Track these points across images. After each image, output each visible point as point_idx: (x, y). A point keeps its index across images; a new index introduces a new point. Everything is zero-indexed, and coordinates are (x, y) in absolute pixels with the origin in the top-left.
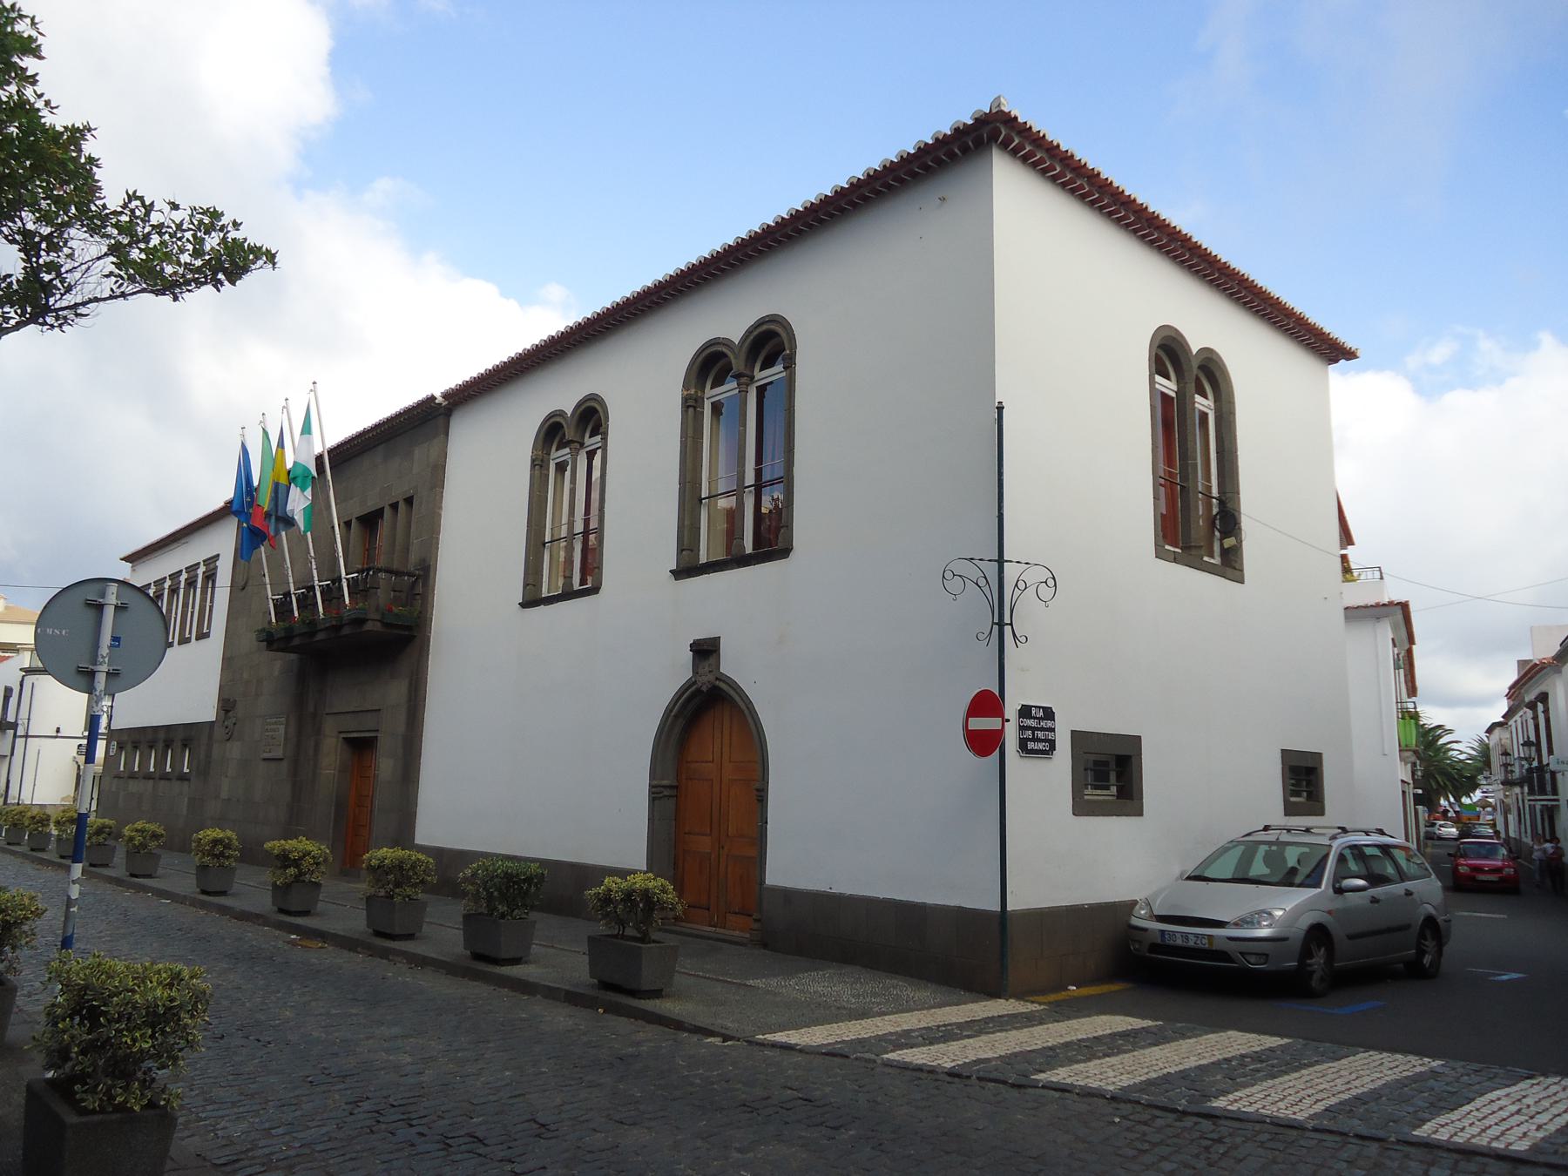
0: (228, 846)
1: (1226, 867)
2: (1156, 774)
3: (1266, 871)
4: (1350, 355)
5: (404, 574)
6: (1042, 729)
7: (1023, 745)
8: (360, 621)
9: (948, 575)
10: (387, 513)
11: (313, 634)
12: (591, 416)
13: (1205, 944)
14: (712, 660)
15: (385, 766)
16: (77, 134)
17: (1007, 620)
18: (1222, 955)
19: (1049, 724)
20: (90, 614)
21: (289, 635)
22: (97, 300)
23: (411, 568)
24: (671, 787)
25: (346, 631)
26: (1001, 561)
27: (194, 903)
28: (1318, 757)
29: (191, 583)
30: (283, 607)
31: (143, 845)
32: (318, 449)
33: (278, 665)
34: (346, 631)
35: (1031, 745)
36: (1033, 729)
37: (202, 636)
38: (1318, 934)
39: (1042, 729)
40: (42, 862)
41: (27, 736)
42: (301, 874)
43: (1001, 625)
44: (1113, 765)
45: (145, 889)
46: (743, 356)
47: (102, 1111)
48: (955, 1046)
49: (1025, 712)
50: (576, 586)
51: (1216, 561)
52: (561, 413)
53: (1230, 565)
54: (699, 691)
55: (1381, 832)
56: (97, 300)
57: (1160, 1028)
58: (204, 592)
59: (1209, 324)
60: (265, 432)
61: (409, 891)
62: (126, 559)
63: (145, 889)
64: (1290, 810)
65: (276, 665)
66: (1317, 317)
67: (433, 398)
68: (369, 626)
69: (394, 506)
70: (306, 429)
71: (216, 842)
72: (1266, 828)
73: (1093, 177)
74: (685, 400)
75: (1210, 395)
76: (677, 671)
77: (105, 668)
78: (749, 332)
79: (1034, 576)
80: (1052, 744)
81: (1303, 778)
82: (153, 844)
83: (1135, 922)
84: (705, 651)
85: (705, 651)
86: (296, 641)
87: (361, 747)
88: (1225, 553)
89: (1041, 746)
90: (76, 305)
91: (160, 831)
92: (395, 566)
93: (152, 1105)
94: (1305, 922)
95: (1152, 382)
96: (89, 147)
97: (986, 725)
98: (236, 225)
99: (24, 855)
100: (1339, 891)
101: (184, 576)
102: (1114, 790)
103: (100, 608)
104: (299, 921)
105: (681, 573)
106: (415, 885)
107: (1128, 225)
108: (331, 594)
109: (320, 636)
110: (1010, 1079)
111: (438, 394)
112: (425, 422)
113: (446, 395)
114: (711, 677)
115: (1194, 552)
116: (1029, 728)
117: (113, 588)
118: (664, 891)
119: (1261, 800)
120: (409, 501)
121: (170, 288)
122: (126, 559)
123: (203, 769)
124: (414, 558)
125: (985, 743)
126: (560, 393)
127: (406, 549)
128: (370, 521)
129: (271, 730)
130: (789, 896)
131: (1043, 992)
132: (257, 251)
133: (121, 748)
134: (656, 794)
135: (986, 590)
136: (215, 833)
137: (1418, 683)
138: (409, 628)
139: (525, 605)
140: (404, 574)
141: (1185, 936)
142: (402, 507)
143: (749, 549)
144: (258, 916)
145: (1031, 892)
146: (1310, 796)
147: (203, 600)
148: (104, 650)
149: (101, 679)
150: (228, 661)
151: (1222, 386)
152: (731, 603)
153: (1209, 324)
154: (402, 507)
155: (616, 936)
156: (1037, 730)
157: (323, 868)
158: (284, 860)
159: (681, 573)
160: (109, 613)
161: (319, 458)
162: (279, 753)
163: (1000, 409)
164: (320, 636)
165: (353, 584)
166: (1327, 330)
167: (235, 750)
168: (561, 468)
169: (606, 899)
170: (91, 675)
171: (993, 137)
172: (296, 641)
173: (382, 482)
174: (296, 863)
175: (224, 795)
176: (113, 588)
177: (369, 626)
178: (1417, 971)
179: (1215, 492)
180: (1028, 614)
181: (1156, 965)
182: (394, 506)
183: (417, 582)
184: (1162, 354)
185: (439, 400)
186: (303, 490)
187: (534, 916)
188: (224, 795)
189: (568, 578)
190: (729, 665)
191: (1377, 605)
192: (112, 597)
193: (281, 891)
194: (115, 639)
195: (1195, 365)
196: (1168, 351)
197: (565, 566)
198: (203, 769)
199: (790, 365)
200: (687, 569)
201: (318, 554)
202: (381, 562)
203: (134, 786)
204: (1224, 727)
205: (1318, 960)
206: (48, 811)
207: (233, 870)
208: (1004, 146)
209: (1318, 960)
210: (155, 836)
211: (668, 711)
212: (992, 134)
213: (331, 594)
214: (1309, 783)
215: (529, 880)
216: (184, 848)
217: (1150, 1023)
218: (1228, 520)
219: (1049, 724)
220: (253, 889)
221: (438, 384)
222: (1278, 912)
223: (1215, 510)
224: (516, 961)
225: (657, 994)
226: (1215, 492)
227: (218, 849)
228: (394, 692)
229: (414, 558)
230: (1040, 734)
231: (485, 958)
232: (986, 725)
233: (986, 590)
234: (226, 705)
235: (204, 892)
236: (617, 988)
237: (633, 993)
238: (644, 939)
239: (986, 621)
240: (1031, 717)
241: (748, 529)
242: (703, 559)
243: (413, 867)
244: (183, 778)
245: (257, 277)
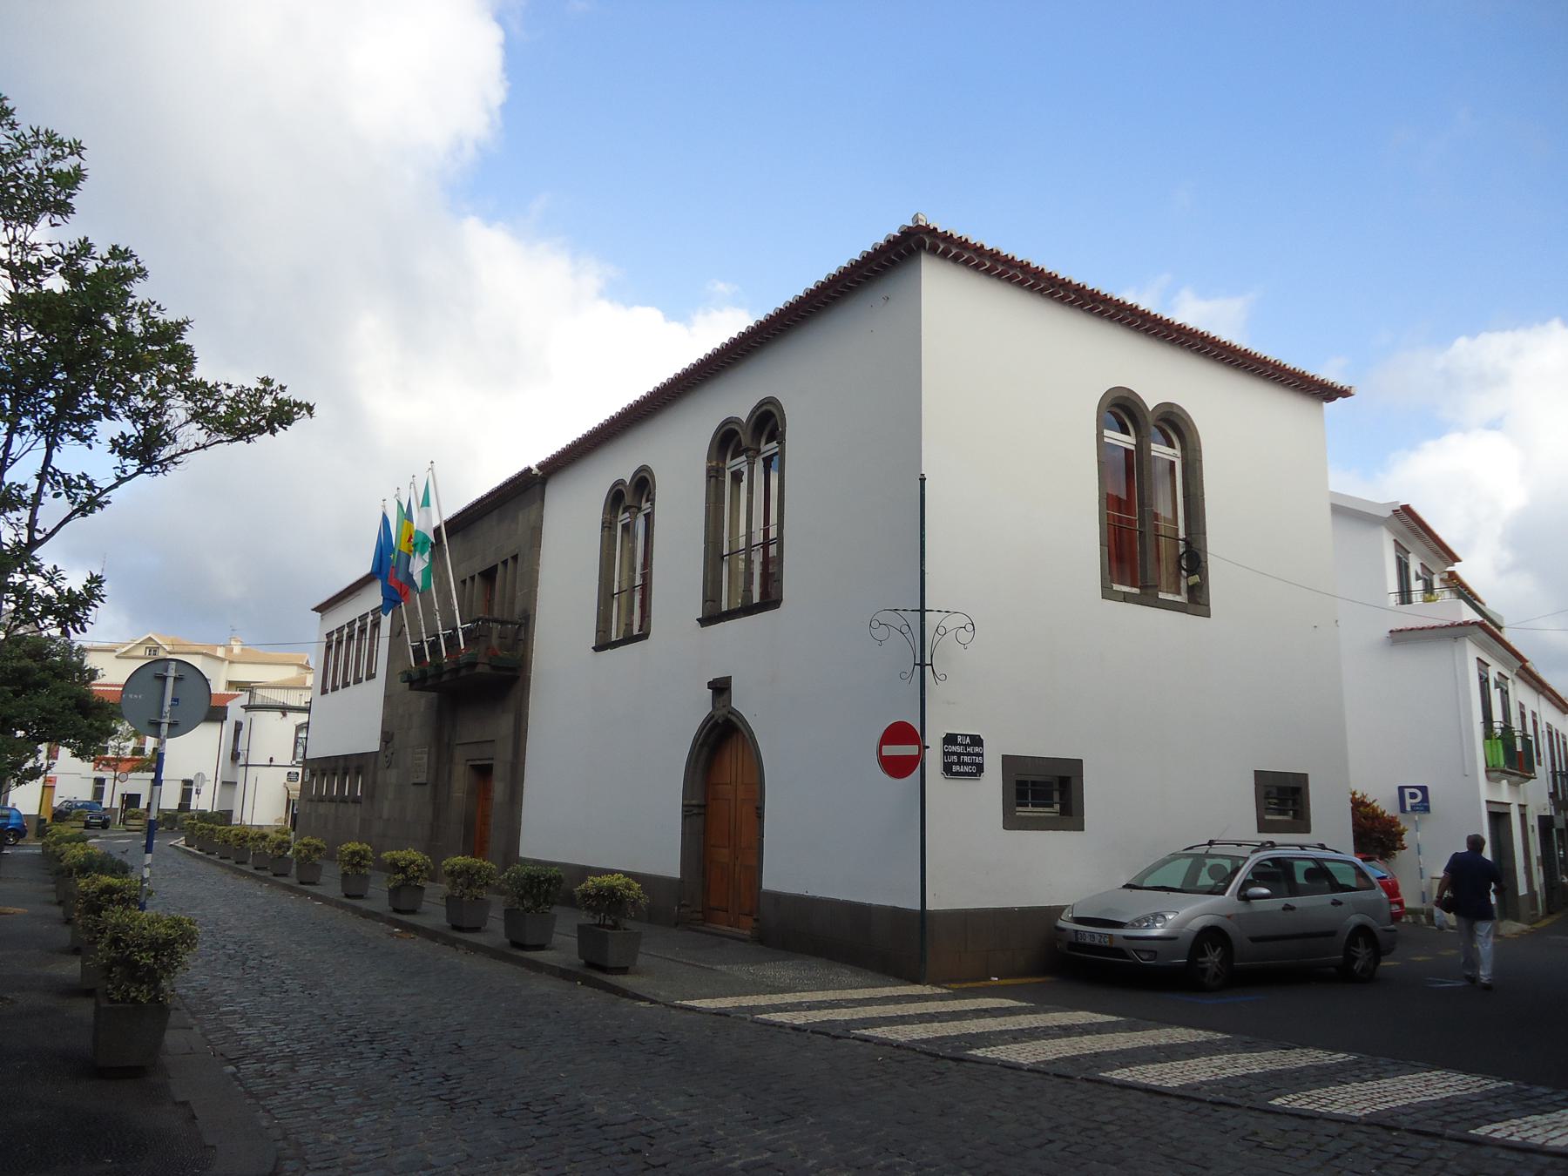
0: (363, 857)
1: (1175, 878)
2: (1094, 792)
3: (1212, 882)
4: (1345, 393)
5: (508, 623)
6: (969, 754)
7: (947, 769)
8: (472, 665)
9: (875, 624)
10: (500, 568)
11: (440, 676)
12: (643, 483)
13: (1106, 942)
14: (725, 696)
15: (499, 789)
16: (180, 327)
17: (928, 661)
18: (1119, 952)
19: (977, 749)
20: (158, 683)
21: (424, 677)
22: (186, 451)
23: (516, 618)
24: (698, 806)
25: (463, 673)
26: (922, 611)
27: (339, 905)
28: (1304, 778)
29: (362, 631)
30: (418, 652)
31: (308, 858)
32: (436, 523)
33: (423, 701)
34: (463, 673)
35: (955, 768)
36: (959, 755)
37: (371, 676)
38: (1211, 935)
39: (969, 754)
40: (243, 873)
41: (247, 765)
42: (408, 879)
43: (922, 665)
44: (1056, 786)
45: (307, 893)
46: (749, 431)
47: (124, 1001)
48: (908, 1028)
49: (950, 739)
50: (636, 632)
51: (1182, 598)
52: (620, 482)
53: (1197, 601)
54: (716, 724)
55: (1322, 847)
56: (186, 451)
57: (1355, 1062)
58: (372, 638)
59: (1160, 378)
60: (400, 505)
61: (475, 891)
62: (316, 609)
63: (307, 893)
64: (1263, 827)
65: (421, 702)
66: (1292, 361)
67: (529, 470)
68: (479, 669)
69: (505, 563)
70: (426, 502)
71: (354, 853)
72: (1211, 843)
73: (1024, 267)
74: (709, 470)
75: (1177, 444)
76: (700, 707)
77: (167, 720)
78: (753, 412)
79: (952, 622)
80: (980, 768)
81: (1283, 797)
82: (316, 857)
83: (1061, 924)
84: (720, 688)
85: (720, 688)
86: (429, 682)
87: (483, 772)
88: (1192, 590)
89: (967, 769)
90: (173, 457)
91: (322, 845)
92: (506, 617)
93: (155, 999)
94: (1198, 924)
95: (1100, 436)
96: (188, 338)
97: (900, 751)
98: (282, 388)
99: (230, 867)
100: (1244, 897)
101: (358, 624)
102: (1057, 807)
103: (165, 678)
104: (405, 918)
105: (706, 621)
106: (480, 887)
107: (1072, 302)
108: (451, 640)
109: (445, 678)
110: (947, 1057)
111: (533, 466)
112: (524, 491)
113: (540, 467)
114: (724, 711)
115: (1150, 591)
116: (954, 753)
117: (173, 665)
118: (629, 888)
119: (1234, 819)
120: (515, 558)
121: (242, 434)
122: (316, 609)
123: (371, 793)
124: (518, 609)
125: (897, 768)
126: (618, 466)
127: (512, 603)
128: (489, 575)
129: (418, 760)
130: (777, 898)
131: (951, 981)
132: (300, 405)
133: (313, 775)
134: (688, 812)
135: (909, 635)
136: (354, 846)
137: (1563, 696)
138: (513, 669)
139: (598, 648)
140: (508, 623)
141: (1092, 935)
142: (510, 562)
143: (756, 599)
144: (377, 914)
145: (950, 893)
146: (1295, 815)
147: (371, 645)
148: (167, 709)
149: (165, 728)
150: (387, 698)
151: (1187, 435)
152: (739, 646)
153: (1160, 378)
154: (510, 562)
155: (598, 925)
156: (963, 756)
157: (425, 875)
158: (395, 867)
159: (706, 621)
160: (170, 682)
161: (437, 531)
162: (423, 779)
163: (923, 480)
164: (445, 678)
165: (466, 632)
166: (1310, 373)
167: (392, 776)
168: (626, 527)
169: (586, 895)
170: (159, 724)
171: (921, 246)
172: (429, 682)
173: (492, 543)
174: (403, 870)
175: (385, 816)
176: (173, 665)
177: (479, 669)
178: (1345, 975)
179: (1182, 534)
180: (944, 654)
181: (1073, 960)
182: (505, 563)
183: (522, 626)
184: (1118, 411)
185: (535, 471)
186: (422, 554)
187: (556, 910)
188: (385, 816)
189: (630, 625)
190: (740, 701)
191: (1453, 625)
192: (172, 673)
193: (395, 892)
194: (175, 700)
195: (1151, 420)
196: (1121, 409)
197: (623, 619)
198: (371, 793)
199: (781, 443)
200: (711, 617)
201: (444, 611)
202: (496, 614)
203: (323, 808)
204: (1171, 751)
205: (1212, 959)
206: (266, 831)
207: (366, 877)
208: (933, 251)
209: (1212, 959)
210: (318, 850)
211: (696, 740)
212: (912, 246)
213: (451, 640)
214: (1295, 802)
215: (549, 880)
216: (331, 857)
217: (1114, 1018)
218: (1194, 559)
219: (977, 749)
220: (378, 893)
221: (533, 456)
222: (1181, 915)
223: (1182, 550)
224: (540, 947)
225: (624, 971)
226: (1182, 534)
227: (357, 860)
228: (505, 724)
229: (518, 609)
230: (966, 759)
231: (521, 945)
232: (900, 751)
233: (909, 635)
234: (387, 737)
235: (347, 896)
236: (597, 968)
237: (604, 969)
238: (615, 927)
239: (909, 659)
240: (955, 743)
241: (746, 584)
242: (725, 608)
243: (478, 872)
244: (356, 801)
245: (301, 424)
